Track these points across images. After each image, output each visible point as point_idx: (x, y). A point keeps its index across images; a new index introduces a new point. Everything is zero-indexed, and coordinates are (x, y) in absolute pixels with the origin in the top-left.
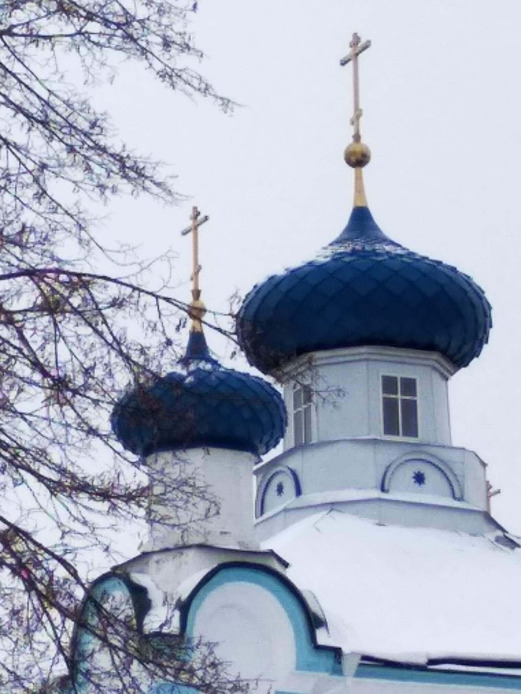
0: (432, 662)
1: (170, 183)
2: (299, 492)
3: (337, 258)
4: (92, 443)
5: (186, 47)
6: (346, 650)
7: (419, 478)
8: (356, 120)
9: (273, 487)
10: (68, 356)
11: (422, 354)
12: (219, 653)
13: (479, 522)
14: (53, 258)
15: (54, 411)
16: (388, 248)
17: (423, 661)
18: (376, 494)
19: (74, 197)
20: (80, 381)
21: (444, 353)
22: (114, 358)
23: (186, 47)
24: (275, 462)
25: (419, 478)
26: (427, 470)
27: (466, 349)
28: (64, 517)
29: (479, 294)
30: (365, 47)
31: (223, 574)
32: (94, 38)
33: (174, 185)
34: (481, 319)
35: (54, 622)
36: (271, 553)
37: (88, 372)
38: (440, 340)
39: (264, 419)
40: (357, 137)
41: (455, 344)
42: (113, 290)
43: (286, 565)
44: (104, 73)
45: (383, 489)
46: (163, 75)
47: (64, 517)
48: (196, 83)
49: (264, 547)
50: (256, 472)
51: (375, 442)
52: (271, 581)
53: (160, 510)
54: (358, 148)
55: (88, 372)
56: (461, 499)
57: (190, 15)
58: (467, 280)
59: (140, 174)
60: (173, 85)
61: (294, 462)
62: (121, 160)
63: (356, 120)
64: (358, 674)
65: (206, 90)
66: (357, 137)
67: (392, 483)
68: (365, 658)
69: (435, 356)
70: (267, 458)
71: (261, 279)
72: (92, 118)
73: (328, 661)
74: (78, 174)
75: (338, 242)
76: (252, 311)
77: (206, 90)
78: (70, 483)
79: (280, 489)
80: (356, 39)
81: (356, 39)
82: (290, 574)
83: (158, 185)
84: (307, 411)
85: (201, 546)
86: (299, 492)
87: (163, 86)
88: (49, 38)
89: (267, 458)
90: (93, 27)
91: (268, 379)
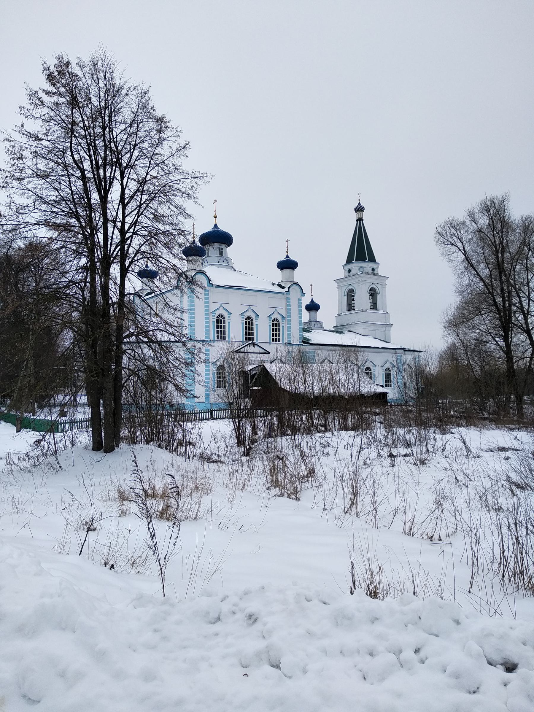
3: (212, 231)
4: (390, 398)
5: (197, 198)
7: (223, 261)
8: (215, 212)
20: (183, 245)
22: (187, 242)
23: (197, 198)
25: (223, 261)
29: (232, 237)
35: (90, 164)
37: (184, 244)
38: (226, 243)
42: (187, 233)
46: (194, 202)
55: (184, 244)
62: (187, 214)
63: (215, 212)
65: (200, 204)
67: (220, 262)
73: (211, 285)
77: (200, 204)
78: (92, 183)
90: (184, 195)
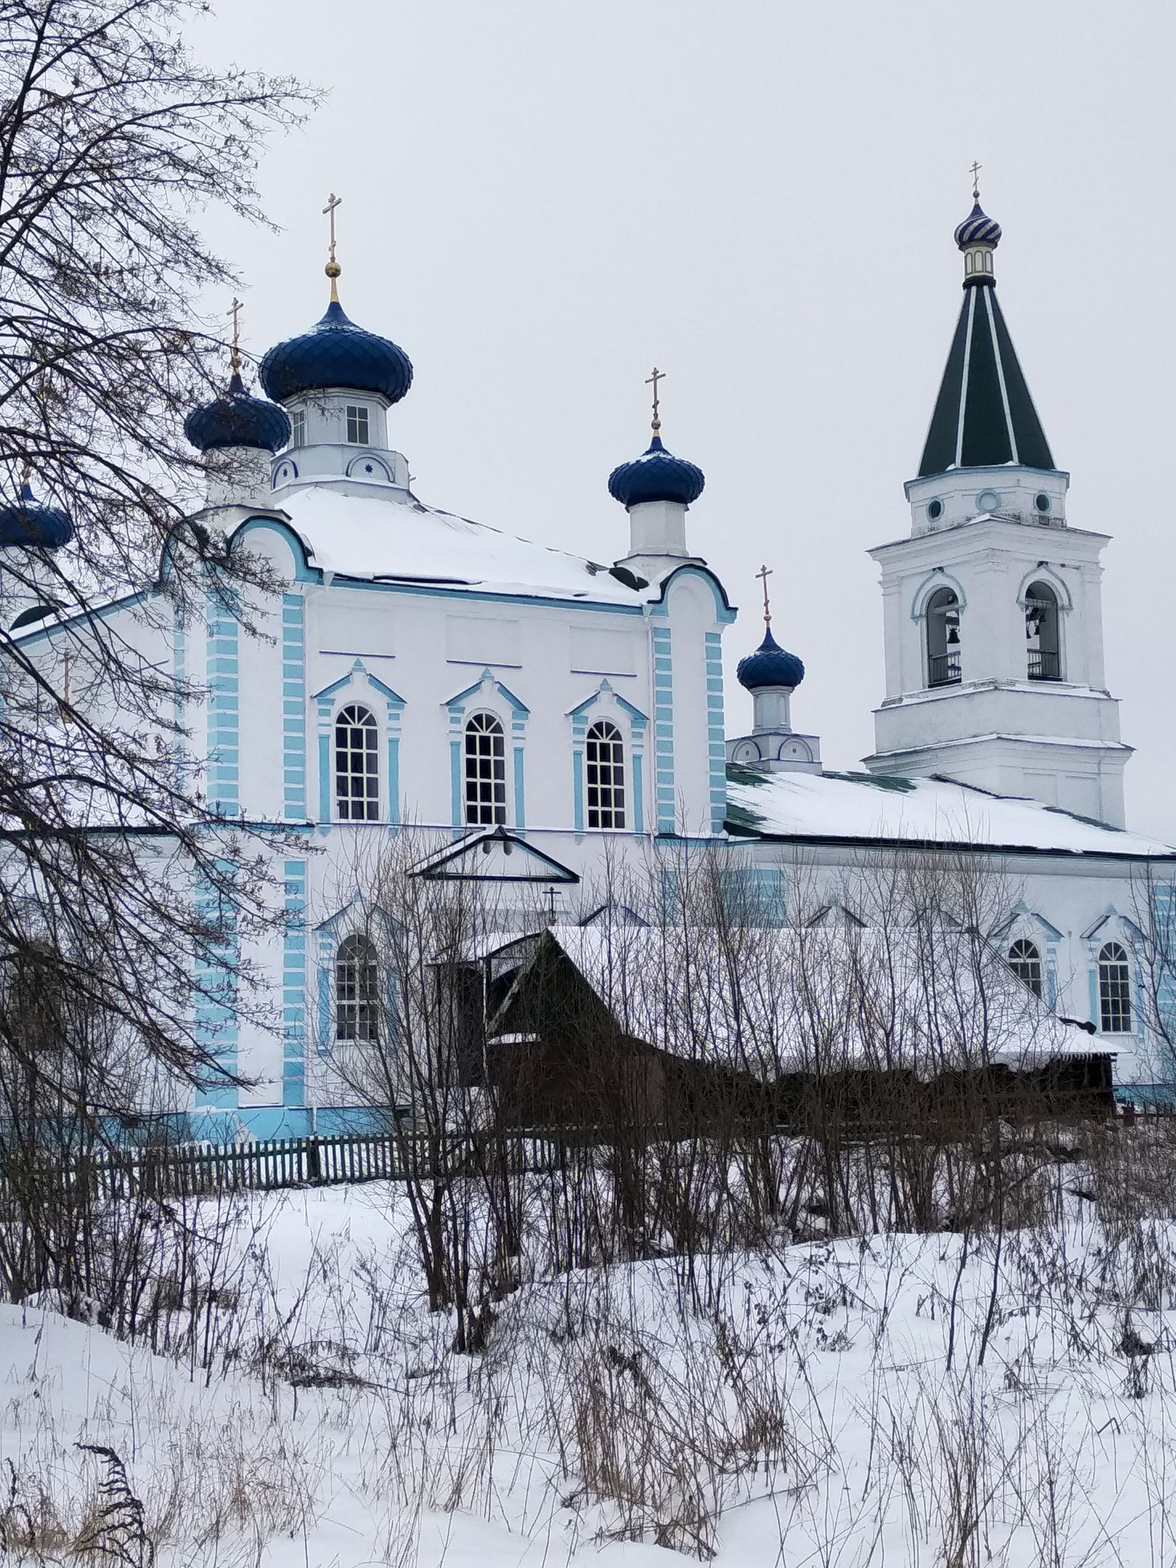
0: (376, 578)
1: (239, 276)
2: (296, 475)
3: (320, 333)
5: (251, 191)
6: (325, 570)
9: (281, 471)
10: (176, 382)
11: (372, 394)
12: (272, 564)
13: (404, 496)
14: (170, 320)
15: (168, 415)
16: (352, 328)
17: (371, 577)
18: (344, 478)
19: (181, 283)
21: (384, 393)
23: (251, 191)
24: (283, 456)
26: (374, 464)
27: (398, 391)
28: (176, 479)
29: (406, 359)
30: (339, 202)
31: (252, 523)
32: (190, 183)
33: (241, 278)
34: (406, 373)
36: (281, 511)
38: (382, 386)
39: (277, 429)
40: (333, 259)
41: (391, 388)
43: (290, 518)
44: (197, 206)
45: (347, 475)
47: (176, 479)
48: (257, 214)
49: (276, 508)
50: (272, 462)
51: (343, 446)
52: (280, 527)
53: (236, 477)
54: (333, 265)
56: (393, 482)
57: (253, 170)
58: (399, 349)
59: (220, 271)
60: (243, 214)
61: (294, 457)
64: (332, 584)
66: (333, 259)
67: (353, 471)
68: (337, 575)
69: (379, 395)
70: (278, 454)
71: (275, 345)
72: (190, 234)
74: (182, 268)
75: (321, 323)
76: (269, 362)
79: (285, 473)
80: (333, 197)
81: (333, 197)
82: (291, 523)
83: (233, 278)
84: (302, 427)
85: (239, 506)
86: (296, 475)
87: (237, 214)
88: (163, 181)
89: (278, 454)
90: (190, 176)
91: (279, 405)
